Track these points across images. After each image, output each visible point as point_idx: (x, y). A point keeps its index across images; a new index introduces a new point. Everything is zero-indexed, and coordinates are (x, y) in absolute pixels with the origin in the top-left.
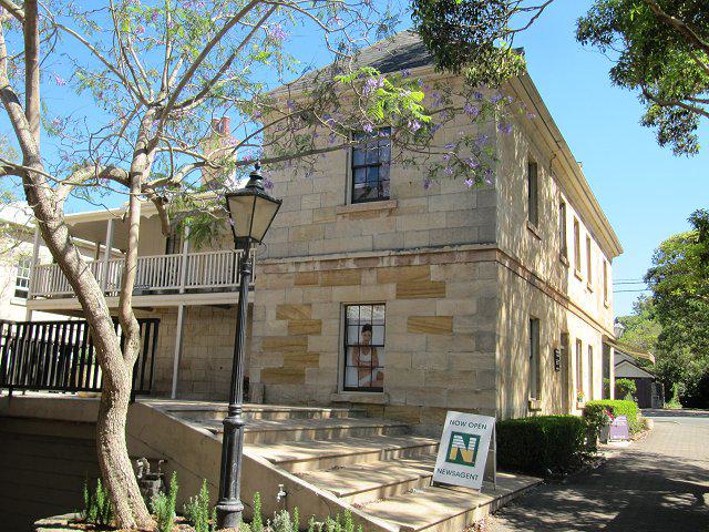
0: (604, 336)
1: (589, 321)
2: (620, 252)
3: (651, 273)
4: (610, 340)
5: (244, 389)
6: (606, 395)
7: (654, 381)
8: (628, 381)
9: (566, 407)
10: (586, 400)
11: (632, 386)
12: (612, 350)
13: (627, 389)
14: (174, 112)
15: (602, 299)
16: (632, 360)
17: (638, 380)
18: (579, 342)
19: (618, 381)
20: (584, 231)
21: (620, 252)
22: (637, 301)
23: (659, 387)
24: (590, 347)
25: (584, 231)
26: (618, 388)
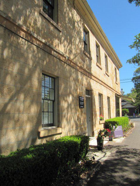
0: (116, 94)
1: (106, 86)
2: (121, 66)
3: (133, 79)
4: (118, 95)
5: (57, 111)
6: (118, 114)
7: (136, 108)
8: (126, 109)
9: (110, 117)
10: (106, 118)
11: (128, 111)
12: (120, 100)
13: (126, 112)
14: (82, 74)
15: (115, 80)
16: (130, 103)
17: (129, 109)
18: (100, 95)
19: (123, 110)
20: (103, 52)
21: (121, 66)
22: (131, 89)
23: (137, 109)
24: (108, 98)
25: (103, 52)
26: (123, 112)
